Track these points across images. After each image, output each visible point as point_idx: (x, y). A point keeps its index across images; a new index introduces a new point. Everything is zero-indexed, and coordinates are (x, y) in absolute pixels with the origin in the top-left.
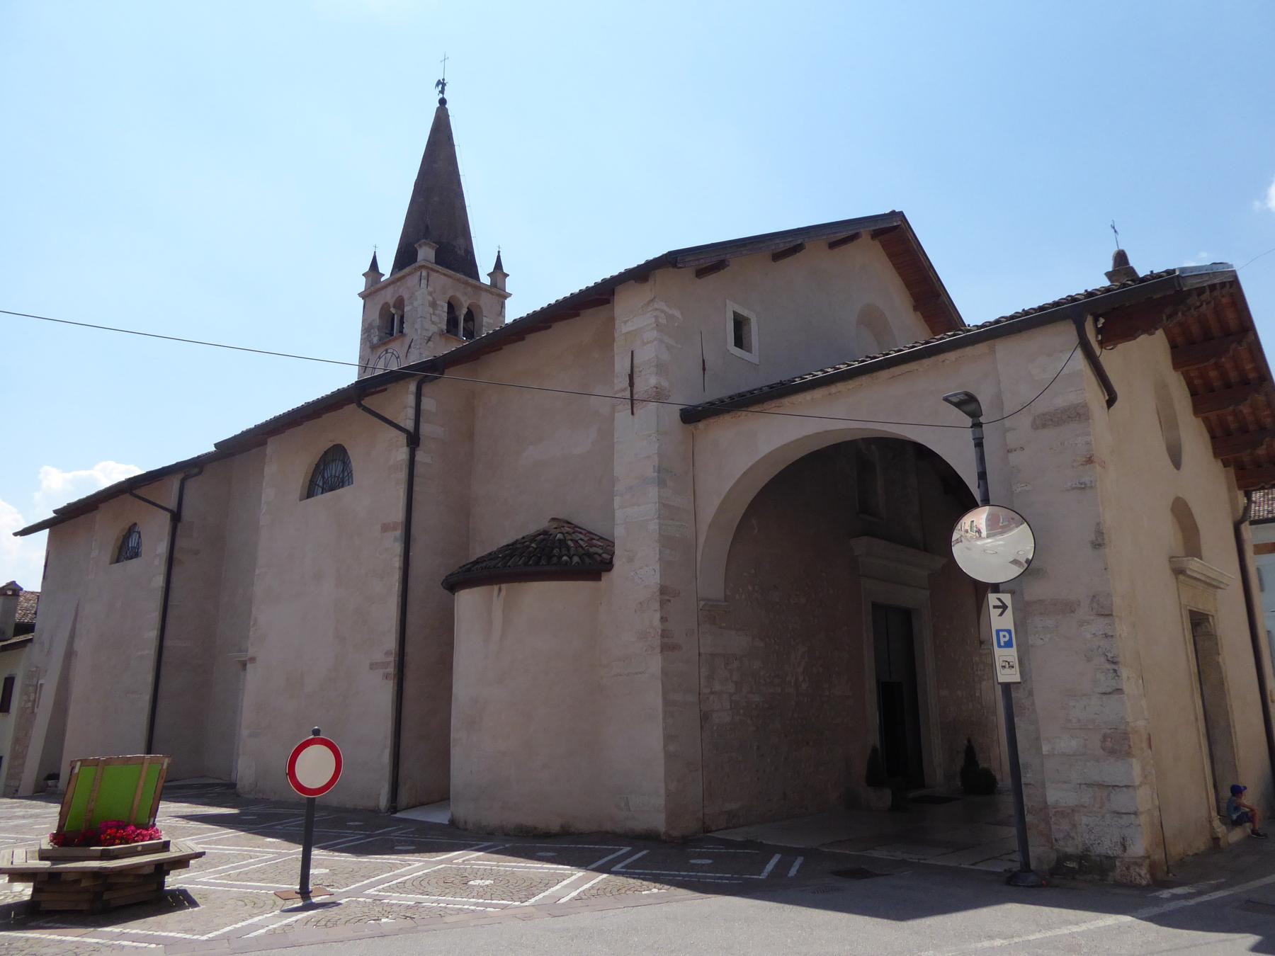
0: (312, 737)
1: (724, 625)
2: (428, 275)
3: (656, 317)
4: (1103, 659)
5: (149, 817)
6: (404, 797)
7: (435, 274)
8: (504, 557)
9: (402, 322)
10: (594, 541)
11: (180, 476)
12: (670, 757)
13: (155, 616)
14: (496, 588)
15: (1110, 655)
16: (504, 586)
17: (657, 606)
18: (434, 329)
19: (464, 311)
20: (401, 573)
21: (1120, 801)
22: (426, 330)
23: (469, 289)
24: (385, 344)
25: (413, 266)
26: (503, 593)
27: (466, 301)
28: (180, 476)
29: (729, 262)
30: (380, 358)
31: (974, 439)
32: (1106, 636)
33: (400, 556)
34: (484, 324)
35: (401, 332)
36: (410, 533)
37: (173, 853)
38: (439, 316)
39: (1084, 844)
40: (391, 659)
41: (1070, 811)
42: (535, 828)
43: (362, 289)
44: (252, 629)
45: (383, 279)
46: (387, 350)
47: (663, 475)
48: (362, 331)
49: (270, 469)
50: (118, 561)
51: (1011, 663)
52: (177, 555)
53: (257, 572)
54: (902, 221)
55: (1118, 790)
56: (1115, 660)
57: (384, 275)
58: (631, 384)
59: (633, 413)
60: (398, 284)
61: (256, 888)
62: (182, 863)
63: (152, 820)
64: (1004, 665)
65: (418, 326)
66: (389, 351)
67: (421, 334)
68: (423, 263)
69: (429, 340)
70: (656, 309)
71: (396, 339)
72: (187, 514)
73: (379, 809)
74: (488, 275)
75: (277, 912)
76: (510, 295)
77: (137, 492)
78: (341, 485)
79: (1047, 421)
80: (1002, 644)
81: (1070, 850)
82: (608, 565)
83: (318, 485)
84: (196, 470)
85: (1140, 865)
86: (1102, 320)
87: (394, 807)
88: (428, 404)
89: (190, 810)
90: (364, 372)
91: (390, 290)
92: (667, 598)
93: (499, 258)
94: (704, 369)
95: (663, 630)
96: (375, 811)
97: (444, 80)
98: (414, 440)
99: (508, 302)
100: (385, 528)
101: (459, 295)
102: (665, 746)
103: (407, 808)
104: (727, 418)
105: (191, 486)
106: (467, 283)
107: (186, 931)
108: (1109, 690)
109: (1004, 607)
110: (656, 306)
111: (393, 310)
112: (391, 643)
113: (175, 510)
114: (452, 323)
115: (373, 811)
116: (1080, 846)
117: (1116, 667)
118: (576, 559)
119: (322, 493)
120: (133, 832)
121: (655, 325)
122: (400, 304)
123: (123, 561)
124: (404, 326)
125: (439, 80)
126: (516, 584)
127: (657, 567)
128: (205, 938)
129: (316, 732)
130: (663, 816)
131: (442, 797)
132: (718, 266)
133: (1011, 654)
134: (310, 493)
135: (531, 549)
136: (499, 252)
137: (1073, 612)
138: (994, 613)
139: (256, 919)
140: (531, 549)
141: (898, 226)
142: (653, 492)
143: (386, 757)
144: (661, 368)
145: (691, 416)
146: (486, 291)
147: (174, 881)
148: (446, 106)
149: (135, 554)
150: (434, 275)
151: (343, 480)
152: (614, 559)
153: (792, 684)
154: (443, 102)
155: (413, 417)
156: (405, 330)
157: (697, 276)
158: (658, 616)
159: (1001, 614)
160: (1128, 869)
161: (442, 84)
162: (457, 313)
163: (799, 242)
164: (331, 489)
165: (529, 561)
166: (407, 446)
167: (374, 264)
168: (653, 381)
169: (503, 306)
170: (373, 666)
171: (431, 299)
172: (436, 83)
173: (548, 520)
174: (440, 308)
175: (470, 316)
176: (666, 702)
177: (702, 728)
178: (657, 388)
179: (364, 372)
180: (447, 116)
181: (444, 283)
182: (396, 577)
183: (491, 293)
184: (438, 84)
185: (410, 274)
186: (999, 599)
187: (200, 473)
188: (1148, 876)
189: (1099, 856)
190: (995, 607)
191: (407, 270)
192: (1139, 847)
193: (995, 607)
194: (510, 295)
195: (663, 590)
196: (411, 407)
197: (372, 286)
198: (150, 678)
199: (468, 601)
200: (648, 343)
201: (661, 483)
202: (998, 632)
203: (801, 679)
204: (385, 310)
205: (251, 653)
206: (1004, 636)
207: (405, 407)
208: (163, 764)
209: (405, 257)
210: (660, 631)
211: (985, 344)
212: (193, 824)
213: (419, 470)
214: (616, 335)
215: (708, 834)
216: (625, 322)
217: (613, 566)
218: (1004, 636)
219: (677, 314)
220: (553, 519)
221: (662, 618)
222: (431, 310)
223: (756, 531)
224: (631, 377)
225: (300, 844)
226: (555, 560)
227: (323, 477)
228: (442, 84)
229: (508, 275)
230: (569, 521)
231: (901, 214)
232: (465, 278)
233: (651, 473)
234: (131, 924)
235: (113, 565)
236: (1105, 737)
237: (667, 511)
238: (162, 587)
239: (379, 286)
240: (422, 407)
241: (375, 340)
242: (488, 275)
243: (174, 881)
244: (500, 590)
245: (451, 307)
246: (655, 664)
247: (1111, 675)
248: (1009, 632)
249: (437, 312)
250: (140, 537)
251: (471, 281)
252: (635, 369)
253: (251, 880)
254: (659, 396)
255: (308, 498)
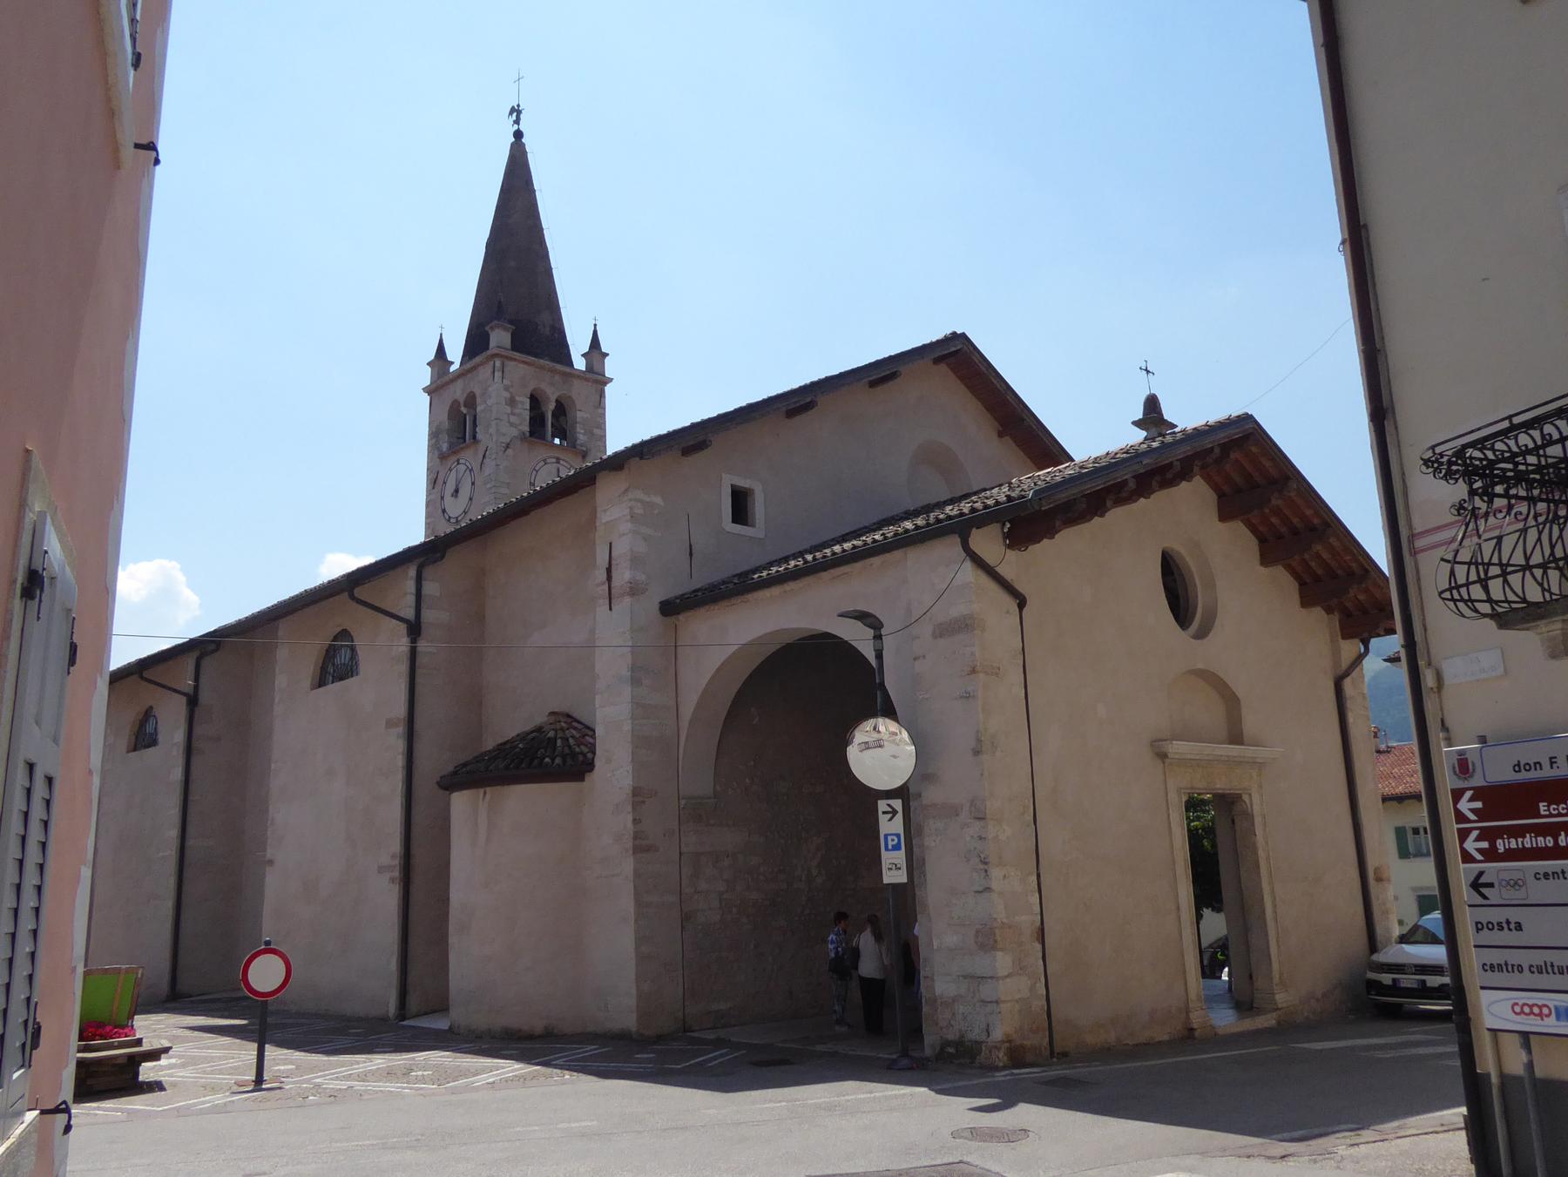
0: (263, 947)
1: (712, 822)
2: (503, 365)
3: (631, 508)
4: (978, 860)
5: (128, 1019)
6: (413, 1003)
7: (513, 363)
8: (489, 759)
9: (475, 424)
10: (587, 738)
11: (195, 654)
12: (641, 959)
13: (174, 813)
14: (481, 791)
15: (982, 856)
16: (488, 789)
17: (629, 808)
18: (514, 432)
19: (552, 406)
20: (405, 773)
21: (986, 991)
22: (504, 435)
23: (557, 377)
24: (454, 453)
25: (484, 355)
26: (488, 796)
27: (553, 394)
28: (195, 654)
29: (710, 441)
30: (450, 470)
31: (875, 650)
32: (981, 838)
33: (403, 754)
34: (578, 420)
35: (474, 437)
36: (412, 728)
37: (146, 1047)
38: (519, 415)
39: (960, 1031)
40: (397, 862)
41: (951, 1001)
42: (520, 1030)
43: (427, 382)
44: (269, 829)
45: (452, 369)
46: (458, 461)
47: (638, 674)
48: (429, 435)
49: (282, 653)
50: (135, 749)
51: (898, 866)
52: (195, 744)
53: (273, 766)
54: (963, 344)
55: (985, 980)
56: (986, 860)
57: (452, 363)
58: (609, 578)
59: (611, 609)
60: (469, 375)
61: (219, 1079)
62: (154, 1055)
63: (130, 1021)
64: (890, 866)
65: (492, 430)
66: (461, 461)
67: (497, 441)
68: (496, 351)
69: (508, 446)
70: (631, 500)
71: (468, 447)
72: (205, 696)
73: (388, 1017)
74: (582, 355)
75: (227, 1094)
76: (611, 380)
77: (145, 674)
78: (350, 674)
79: (946, 630)
80: (890, 847)
81: (950, 1037)
82: (589, 766)
83: (330, 673)
84: (213, 647)
85: (998, 1049)
86: (1008, 525)
87: (403, 1012)
88: (430, 588)
89: (203, 1022)
90: (433, 488)
91: (459, 384)
92: (641, 799)
93: (595, 333)
94: (691, 554)
95: (635, 833)
96: (384, 1019)
97: (518, 106)
98: (414, 629)
99: (608, 389)
100: (390, 724)
101: (543, 386)
102: (637, 949)
103: (417, 1015)
104: (702, 612)
105: (207, 663)
106: (553, 371)
107: (147, 1105)
108: (981, 889)
109: (894, 812)
110: (630, 495)
111: (464, 410)
112: (396, 846)
113: (192, 692)
114: (537, 421)
115: (382, 1019)
116: (958, 1034)
117: (986, 867)
118: (558, 761)
119: (333, 682)
120: (111, 1031)
121: (629, 517)
122: (471, 401)
123: (140, 750)
124: (477, 429)
125: (513, 107)
126: (499, 788)
127: (630, 768)
128: (161, 1109)
129: (268, 943)
130: (634, 1016)
131: (442, 1007)
132: (700, 446)
133: (900, 857)
134: (321, 683)
135: (517, 750)
136: (595, 325)
137: (957, 815)
138: (883, 819)
139: (207, 1098)
140: (517, 750)
141: (959, 350)
142: (627, 691)
143: (393, 965)
144: (636, 561)
145: (670, 608)
146: (579, 377)
147: (147, 1071)
148: (523, 140)
149: (153, 742)
150: (510, 365)
151: (347, 672)
152: (595, 759)
153: (803, 879)
154: (518, 135)
155: (413, 604)
156: (479, 436)
157: (683, 455)
158: (630, 818)
159: (890, 820)
160: (990, 1052)
161: (516, 112)
162: (544, 409)
163: (808, 400)
164: (341, 679)
165: (511, 764)
166: (408, 636)
167: (441, 350)
168: (627, 575)
169: (602, 395)
170: (381, 869)
171: (507, 395)
172: (509, 109)
173: (547, 714)
174: (520, 406)
175: (561, 409)
176: (639, 903)
177: (682, 928)
178: (631, 583)
179: (433, 488)
180: (524, 153)
181: (523, 374)
182: (399, 777)
183: (587, 380)
184: (511, 113)
185: (482, 364)
186: (889, 805)
187: (216, 650)
188: (1005, 1058)
189: (970, 1041)
190: (884, 813)
191: (478, 359)
192: (998, 1034)
193: (884, 813)
194: (611, 380)
195: (636, 792)
196: (411, 593)
197: (439, 378)
198: (172, 882)
199: (460, 802)
200: (624, 534)
201: (635, 681)
202: (886, 836)
203: (815, 872)
204: (454, 410)
205: (269, 856)
206: (893, 840)
207: (406, 594)
208: (137, 973)
209: (476, 342)
210: (632, 833)
211: (900, 551)
212: (197, 1034)
213: (420, 660)
214: (598, 524)
215: (689, 1034)
216: (605, 511)
217: (594, 766)
218: (893, 840)
219: (658, 500)
220: (552, 713)
221: (634, 820)
222: (508, 410)
223: (757, 719)
224: (609, 570)
225: (253, 1041)
226: (536, 762)
227: (334, 664)
228: (516, 112)
229: (607, 355)
230: (570, 714)
231: (963, 335)
232: (551, 364)
233: (626, 673)
234: (107, 1102)
235: (130, 754)
236: (978, 932)
237: (640, 709)
238: (181, 781)
239: (446, 378)
240: (423, 593)
241: (445, 447)
242: (582, 355)
243: (147, 1071)
244: (485, 793)
245: (535, 401)
246: (628, 866)
247: (983, 874)
248: (898, 836)
249: (517, 411)
250: (157, 722)
251: (559, 367)
252: (613, 562)
253: (223, 1074)
254: (634, 590)
255: (320, 686)
